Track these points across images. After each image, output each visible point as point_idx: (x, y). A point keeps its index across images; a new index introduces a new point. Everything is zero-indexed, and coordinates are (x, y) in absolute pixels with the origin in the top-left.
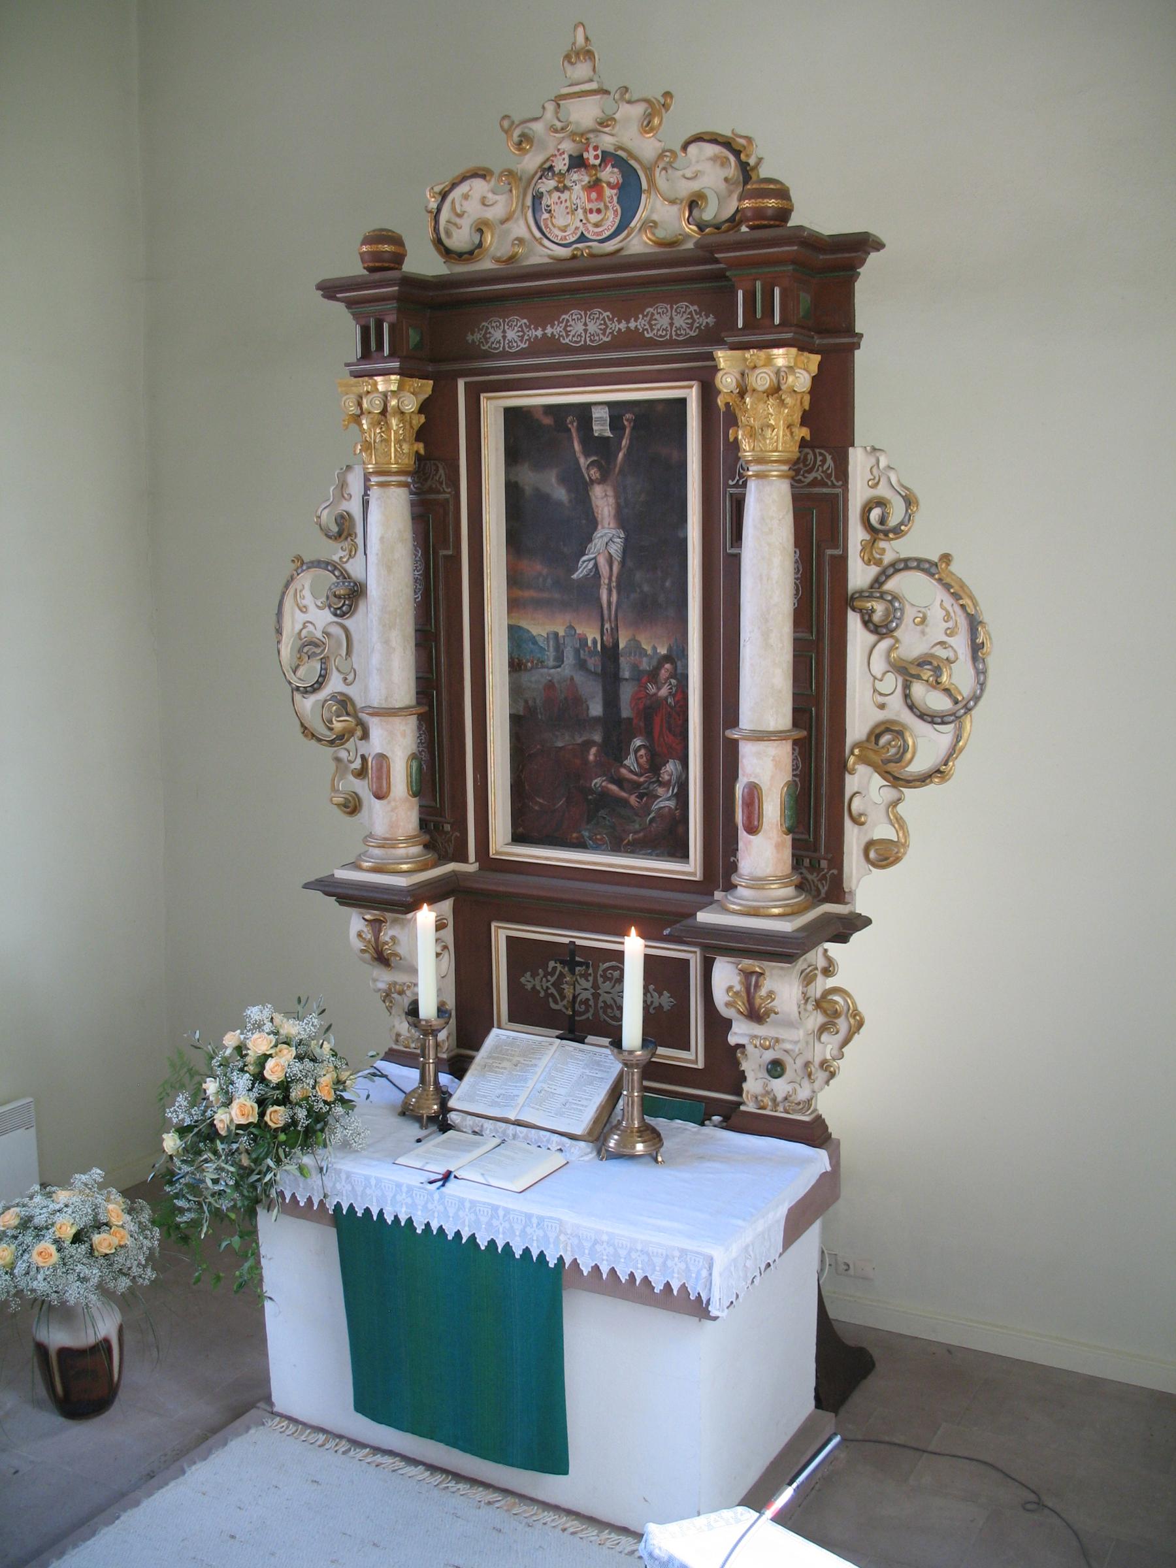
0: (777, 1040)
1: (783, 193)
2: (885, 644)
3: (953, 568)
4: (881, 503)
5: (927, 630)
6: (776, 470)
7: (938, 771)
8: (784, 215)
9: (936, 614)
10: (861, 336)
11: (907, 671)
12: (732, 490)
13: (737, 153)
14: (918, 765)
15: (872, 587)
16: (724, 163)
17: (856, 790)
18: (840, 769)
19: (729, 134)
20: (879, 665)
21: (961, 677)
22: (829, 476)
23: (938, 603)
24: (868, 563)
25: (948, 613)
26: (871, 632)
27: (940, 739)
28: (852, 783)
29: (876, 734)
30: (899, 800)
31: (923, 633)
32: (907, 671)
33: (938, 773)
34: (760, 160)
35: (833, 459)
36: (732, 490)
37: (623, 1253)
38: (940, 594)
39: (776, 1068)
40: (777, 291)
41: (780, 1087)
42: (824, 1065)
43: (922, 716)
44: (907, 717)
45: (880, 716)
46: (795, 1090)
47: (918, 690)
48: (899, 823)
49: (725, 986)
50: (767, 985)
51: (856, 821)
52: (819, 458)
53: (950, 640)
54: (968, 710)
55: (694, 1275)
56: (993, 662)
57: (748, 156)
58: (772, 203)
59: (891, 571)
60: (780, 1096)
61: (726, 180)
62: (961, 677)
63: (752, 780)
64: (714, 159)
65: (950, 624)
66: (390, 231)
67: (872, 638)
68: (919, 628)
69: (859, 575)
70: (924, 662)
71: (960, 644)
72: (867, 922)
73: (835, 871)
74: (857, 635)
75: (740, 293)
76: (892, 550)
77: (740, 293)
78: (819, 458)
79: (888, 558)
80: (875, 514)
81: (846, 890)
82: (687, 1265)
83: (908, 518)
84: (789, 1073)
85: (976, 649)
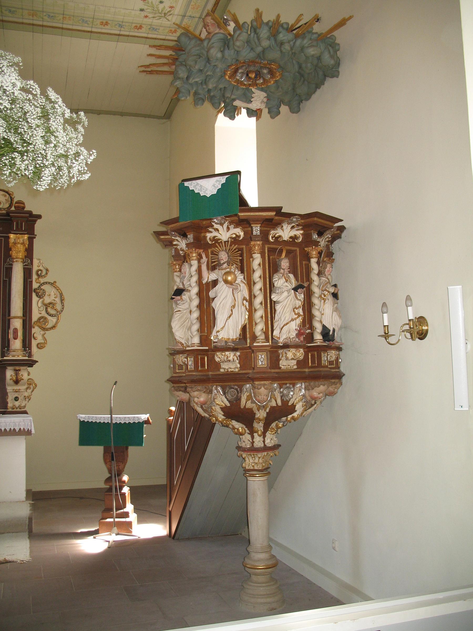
0: (20, 389)
1: (24, 204)
2: (41, 300)
3: (57, 284)
4: (41, 270)
5: (50, 297)
6: (20, 260)
7: (54, 327)
8: (24, 208)
9: (52, 294)
10: (36, 235)
11: (46, 306)
12: (6, 266)
13: (9, 195)
14: (50, 325)
15: (38, 287)
16: (5, 196)
17: (34, 332)
18: (31, 327)
19: (7, 190)
20: (40, 304)
21: (59, 307)
22: (29, 264)
23: (53, 291)
24: (37, 283)
25: (55, 294)
26: (38, 297)
27: (54, 320)
28: (33, 331)
29: (40, 319)
30: (45, 334)
31: (50, 298)
32: (46, 306)
33: (53, 327)
34: (14, 197)
35: (30, 260)
36: (6, 266)
37: (8, 424)
38: (54, 290)
39: (16, 399)
40: (24, 223)
41: (17, 404)
42: (28, 397)
43: (50, 315)
44: (46, 316)
45: (40, 315)
46: (21, 404)
47: (49, 310)
48: (45, 339)
49: (10, 375)
50: (21, 373)
51: (35, 339)
52: (27, 260)
53: (56, 299)
54: (60, 313)
55: (26, 425)
56: (65, 303)
57: (12, 195)
58: (22, 205)
59: (45, 283)
60: (17, 406)
61: (6, 200)
62: (59, 307)
63: (15, 327)
64: (3, 195)
65: (55, 296)
66: (22, 201)
67: (38, 299)
68: (49, 297)
69: (35, 285)
70: (50, 303)
71: (58, 300)
72: (37, 362)
73: (30, 351)
74: (35, 298)
75: (15, 223)
76: (42, 280)
77: (15, 223)
78: (27, 260)
79: (42, 282)
80: (40, 272)
81: (32, 355)
82: (25, 423)
83: (47, 274)
84: (20, 400)
85: (62, 300)
